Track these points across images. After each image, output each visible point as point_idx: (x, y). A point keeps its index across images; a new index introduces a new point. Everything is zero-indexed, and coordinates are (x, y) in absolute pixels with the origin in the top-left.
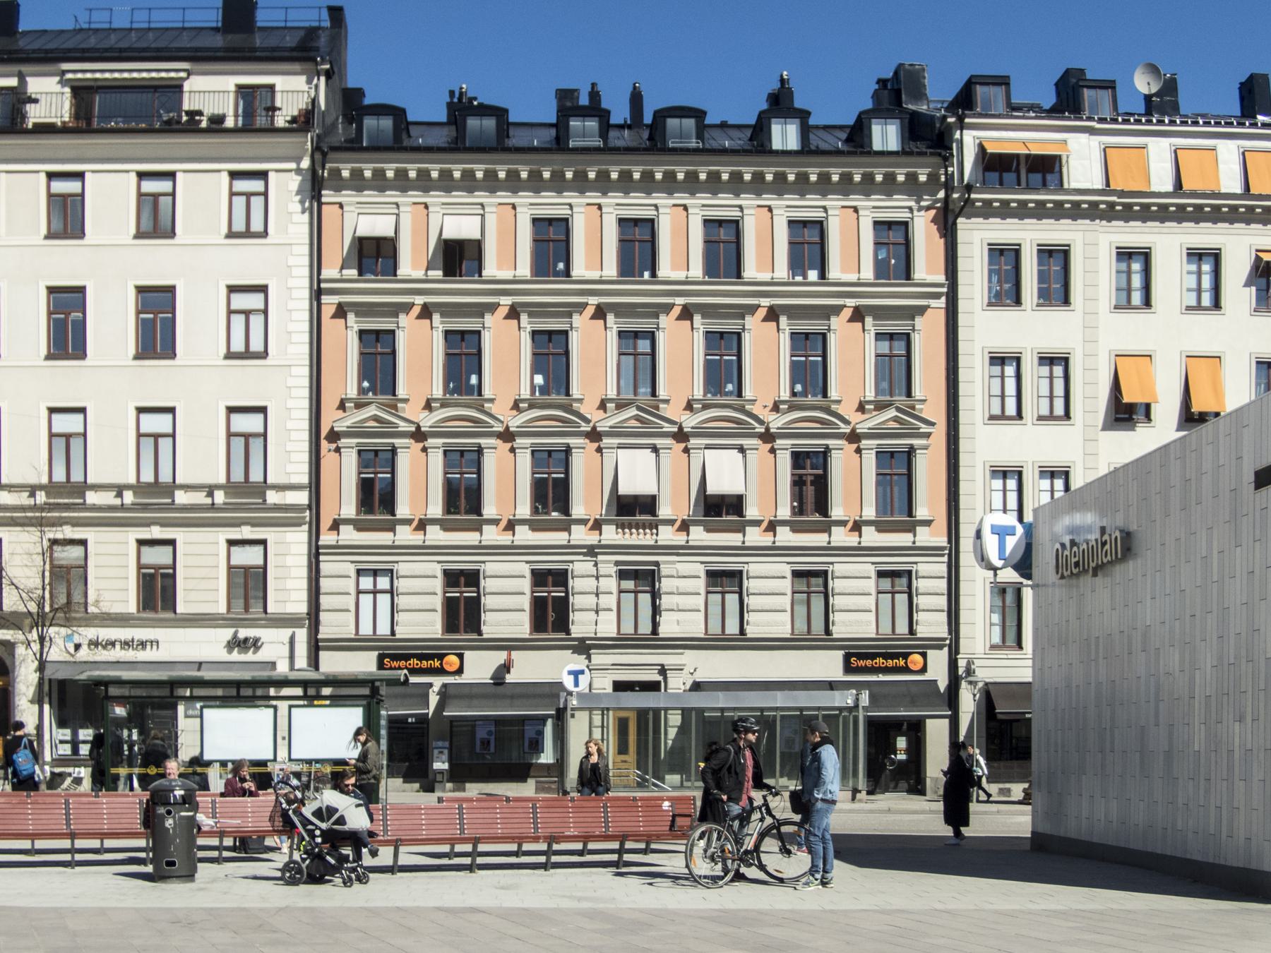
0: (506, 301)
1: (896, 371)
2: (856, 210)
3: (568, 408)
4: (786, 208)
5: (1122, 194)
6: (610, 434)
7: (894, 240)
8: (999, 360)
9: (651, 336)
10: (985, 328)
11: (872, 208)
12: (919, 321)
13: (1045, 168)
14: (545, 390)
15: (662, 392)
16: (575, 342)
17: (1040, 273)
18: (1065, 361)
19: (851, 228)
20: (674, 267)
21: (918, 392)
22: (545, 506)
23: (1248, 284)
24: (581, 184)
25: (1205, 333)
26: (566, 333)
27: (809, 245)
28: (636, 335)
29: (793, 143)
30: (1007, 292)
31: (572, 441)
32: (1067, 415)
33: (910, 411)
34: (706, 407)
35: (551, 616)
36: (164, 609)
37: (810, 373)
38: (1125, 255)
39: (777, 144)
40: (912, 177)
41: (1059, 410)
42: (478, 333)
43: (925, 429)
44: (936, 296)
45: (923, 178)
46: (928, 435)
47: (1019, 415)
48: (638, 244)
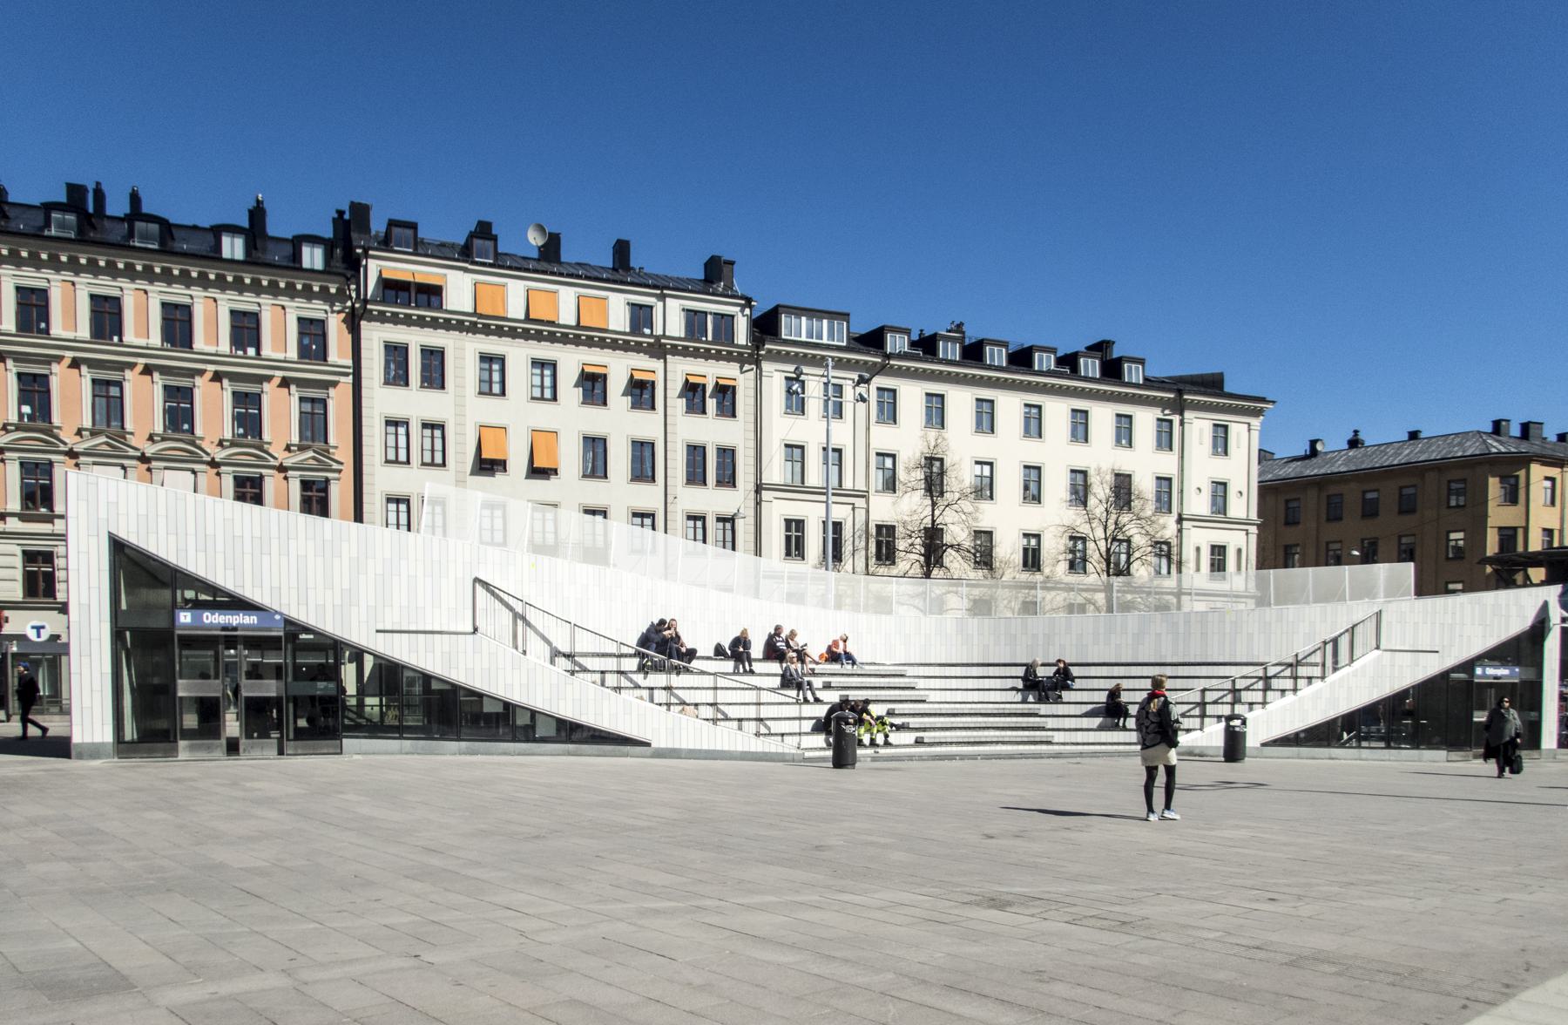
0: (69, 354)
1: (314, 424)
2: (73, 284)
3: (49, 432)
4: (228, 302)
5: (481, 316)
6: (84, 454)
7: (313, 336)
8: (392, 423)
9: (119, 384)
10: (381, 400)
11: (296, 309)
12: (332, 391)
13: (431, 294)
14: (31, 417)
15: (129, 426)
16: (55, 383)
17: (423, 365)
18: (442, 427)
19: (280, 323)
20: (207, 343)
21: (332, 441)
22: (34, 503)
23: (576, 386)
24: (273, 290)
25: (544, 415)
26: (46, 376)
27: (246, 329)
28: (108, 383)
29: (239, 254)
30: (397, 372)
31: (53, 457)
32: (444, 464)
33: (326, 452)
34: (164, 439)
35: (42, 585)
36: (45, 596)
37: (249, 419)
38: (487, 359)
39: (306, 264)
40: (324, 289)
41: (438, 459)
42: (46, 376)
43: (335, 466)
44: (347, 374)
45: (333, 291)
46: (340, 471)
47: (408, 462)
48: (107, 317)
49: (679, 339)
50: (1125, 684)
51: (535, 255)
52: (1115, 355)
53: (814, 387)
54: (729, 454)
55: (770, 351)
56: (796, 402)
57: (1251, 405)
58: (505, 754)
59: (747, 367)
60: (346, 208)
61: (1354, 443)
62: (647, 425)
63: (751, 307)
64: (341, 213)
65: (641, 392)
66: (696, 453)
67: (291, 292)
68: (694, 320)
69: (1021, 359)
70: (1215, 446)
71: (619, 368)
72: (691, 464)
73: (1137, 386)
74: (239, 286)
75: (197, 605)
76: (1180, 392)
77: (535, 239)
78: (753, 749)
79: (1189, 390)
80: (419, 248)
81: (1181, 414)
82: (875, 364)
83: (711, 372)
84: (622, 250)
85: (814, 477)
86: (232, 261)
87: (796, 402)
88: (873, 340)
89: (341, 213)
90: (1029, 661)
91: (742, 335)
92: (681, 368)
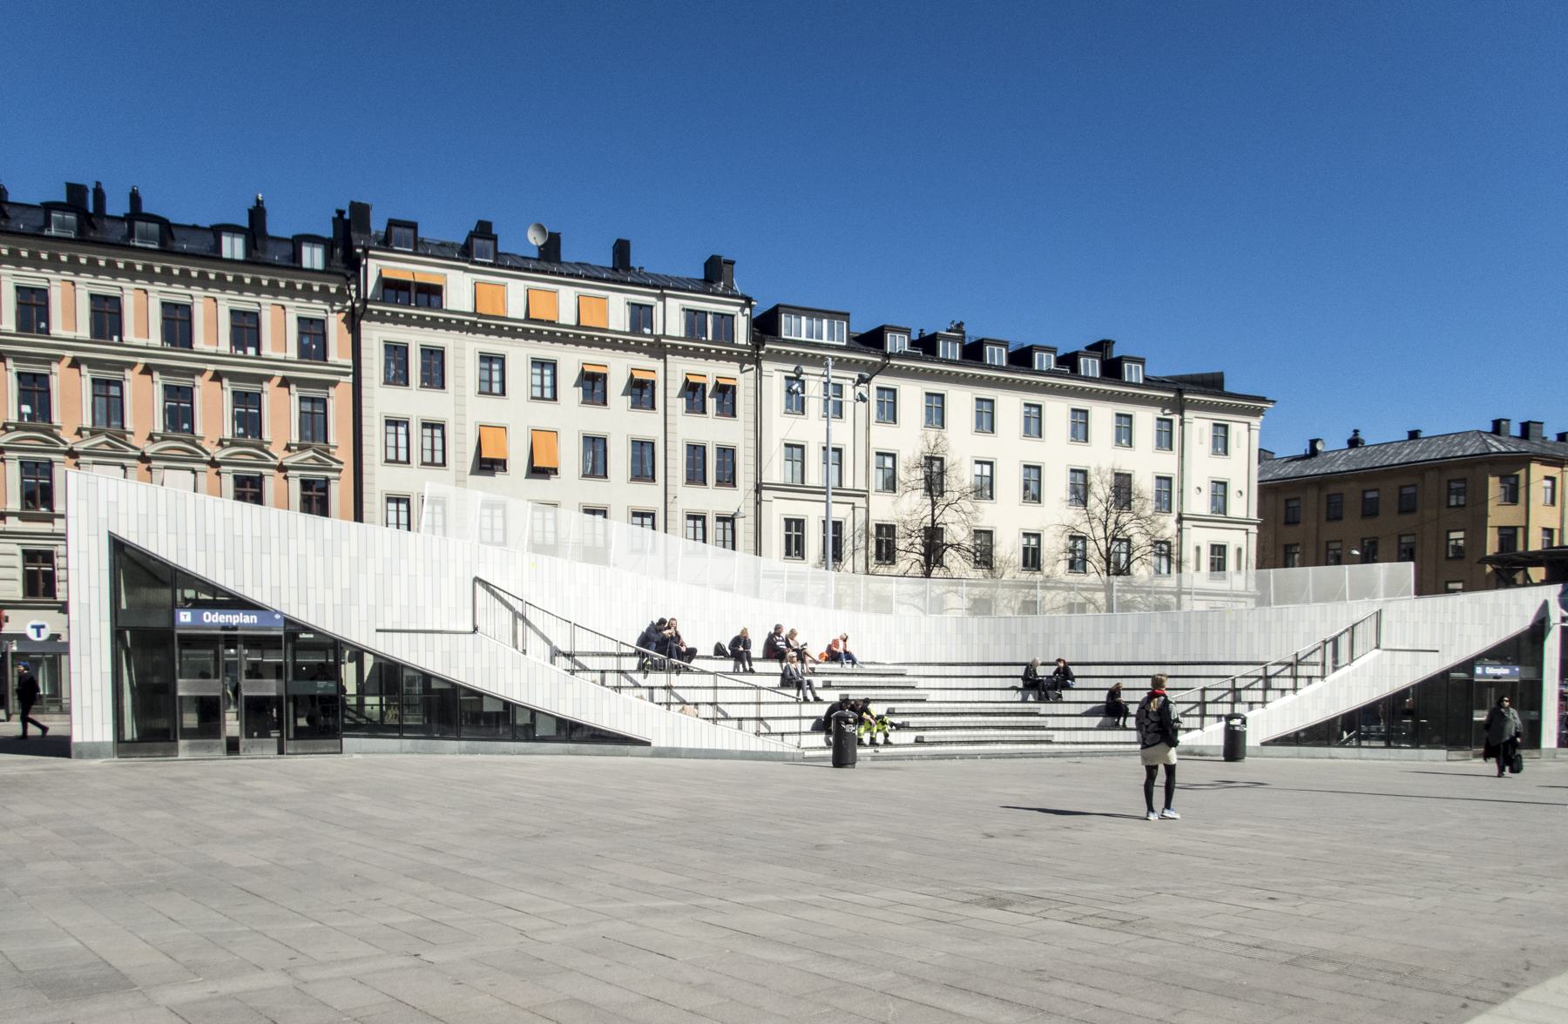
0: (69, 354)
1: (314, 424)
2: (73, 283)
3: (49, 432)
4: (228, 301)
5: (481, 316)
6: (84, 454)
7: (313, 336)
8: (392, 422)
9: (119, 384)
10: (381, 400)
11: (296, 308)
12: (332, 391)
13: (431, 293)
14: (31, 417)
15: (129, 426)
16: (55, 383)
17: (423, 365)
18: (442, 427)
19: (280, 322)
20: (207, 342)
21: (332, 441)
22: (34, 502)
23: (576, 385)
24: (273, 290)
25: (544, 415)
26: (46, 376)
27: (246, 329)
28: (108, 383)
29: (239, 254)
30: (397, 372)
31: (53, 457)
32: (444, 464)
33: (326, 452)
34: (164, 439)
35: (42, 585)
37: (249, 419)
38: (487, 358)
39: (306, 263)
40: (324, 289)
41: (438, 459)
42: (46, 376)
43: (335, 466)
44: (347, 374)
45: (333, 290)
46: (340, 471)
47: (408, 462)
48: (107, 316)
49: (679, 339)
50: (1125, 683)
51: (535, 254)
52: (1115, 355)
53: (814, 387)
54: (729, 453)
55: (770, 351)
56: (796, 402)
57: (1251, 405)
58: (505, 753)
59: (747, 366)
60: (346, 208)
61: (1354, 443)
62: (647, 425)
63: (751, 307)
64: (341, 213)
65: (641, 392)
66: (696, 453)
67: (291, 292)
68: (694, 320)
69: (1021, 358)
70: (1215, 446)
71: (619, 367)
72: (691, 464)
73: (1137, 385)
74: (239, 286)
75: (197, 604)
76: (1180, 392)
77: (535, 239)
78: (753, 749)
79: (1189, 390)
80: (419, 247)
81: (1181, 414)
82: (875, 363)
83: (711, 371)
84: (622, 250)
85: (814, 477)
86: (232, 261)
87: (796, 402)
88: (873, 340)
89: (341, 213)
90: (1029, 660)
91: (742, 335)
92: (681, 368)
